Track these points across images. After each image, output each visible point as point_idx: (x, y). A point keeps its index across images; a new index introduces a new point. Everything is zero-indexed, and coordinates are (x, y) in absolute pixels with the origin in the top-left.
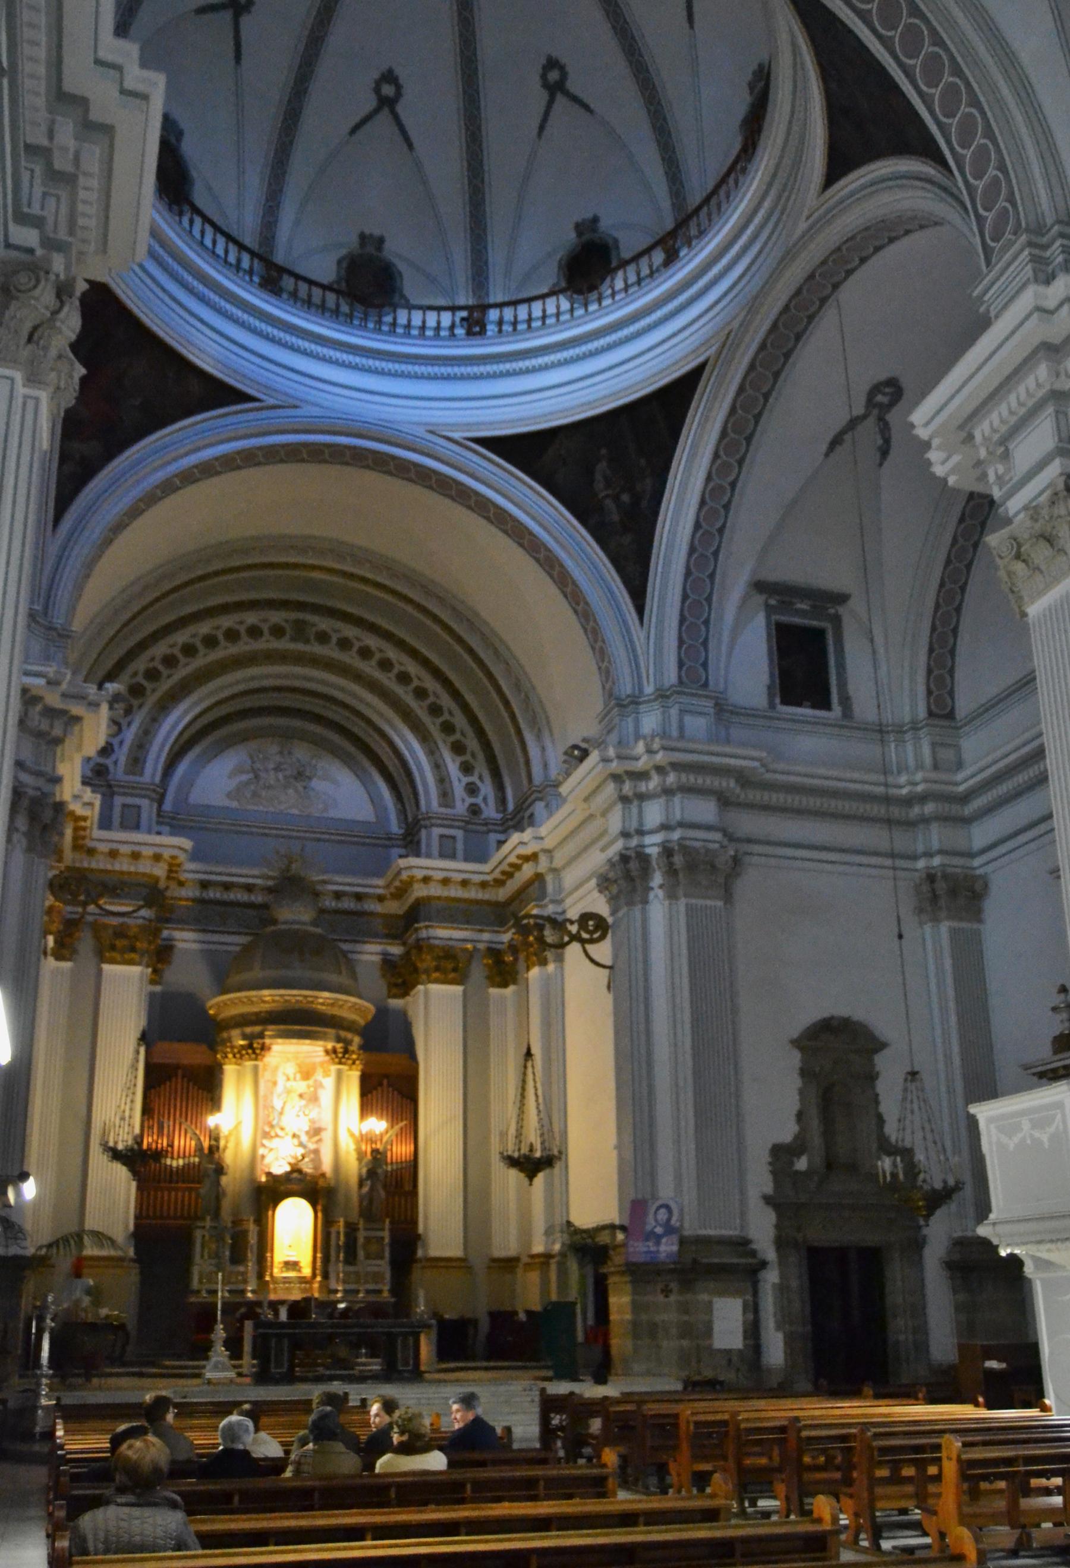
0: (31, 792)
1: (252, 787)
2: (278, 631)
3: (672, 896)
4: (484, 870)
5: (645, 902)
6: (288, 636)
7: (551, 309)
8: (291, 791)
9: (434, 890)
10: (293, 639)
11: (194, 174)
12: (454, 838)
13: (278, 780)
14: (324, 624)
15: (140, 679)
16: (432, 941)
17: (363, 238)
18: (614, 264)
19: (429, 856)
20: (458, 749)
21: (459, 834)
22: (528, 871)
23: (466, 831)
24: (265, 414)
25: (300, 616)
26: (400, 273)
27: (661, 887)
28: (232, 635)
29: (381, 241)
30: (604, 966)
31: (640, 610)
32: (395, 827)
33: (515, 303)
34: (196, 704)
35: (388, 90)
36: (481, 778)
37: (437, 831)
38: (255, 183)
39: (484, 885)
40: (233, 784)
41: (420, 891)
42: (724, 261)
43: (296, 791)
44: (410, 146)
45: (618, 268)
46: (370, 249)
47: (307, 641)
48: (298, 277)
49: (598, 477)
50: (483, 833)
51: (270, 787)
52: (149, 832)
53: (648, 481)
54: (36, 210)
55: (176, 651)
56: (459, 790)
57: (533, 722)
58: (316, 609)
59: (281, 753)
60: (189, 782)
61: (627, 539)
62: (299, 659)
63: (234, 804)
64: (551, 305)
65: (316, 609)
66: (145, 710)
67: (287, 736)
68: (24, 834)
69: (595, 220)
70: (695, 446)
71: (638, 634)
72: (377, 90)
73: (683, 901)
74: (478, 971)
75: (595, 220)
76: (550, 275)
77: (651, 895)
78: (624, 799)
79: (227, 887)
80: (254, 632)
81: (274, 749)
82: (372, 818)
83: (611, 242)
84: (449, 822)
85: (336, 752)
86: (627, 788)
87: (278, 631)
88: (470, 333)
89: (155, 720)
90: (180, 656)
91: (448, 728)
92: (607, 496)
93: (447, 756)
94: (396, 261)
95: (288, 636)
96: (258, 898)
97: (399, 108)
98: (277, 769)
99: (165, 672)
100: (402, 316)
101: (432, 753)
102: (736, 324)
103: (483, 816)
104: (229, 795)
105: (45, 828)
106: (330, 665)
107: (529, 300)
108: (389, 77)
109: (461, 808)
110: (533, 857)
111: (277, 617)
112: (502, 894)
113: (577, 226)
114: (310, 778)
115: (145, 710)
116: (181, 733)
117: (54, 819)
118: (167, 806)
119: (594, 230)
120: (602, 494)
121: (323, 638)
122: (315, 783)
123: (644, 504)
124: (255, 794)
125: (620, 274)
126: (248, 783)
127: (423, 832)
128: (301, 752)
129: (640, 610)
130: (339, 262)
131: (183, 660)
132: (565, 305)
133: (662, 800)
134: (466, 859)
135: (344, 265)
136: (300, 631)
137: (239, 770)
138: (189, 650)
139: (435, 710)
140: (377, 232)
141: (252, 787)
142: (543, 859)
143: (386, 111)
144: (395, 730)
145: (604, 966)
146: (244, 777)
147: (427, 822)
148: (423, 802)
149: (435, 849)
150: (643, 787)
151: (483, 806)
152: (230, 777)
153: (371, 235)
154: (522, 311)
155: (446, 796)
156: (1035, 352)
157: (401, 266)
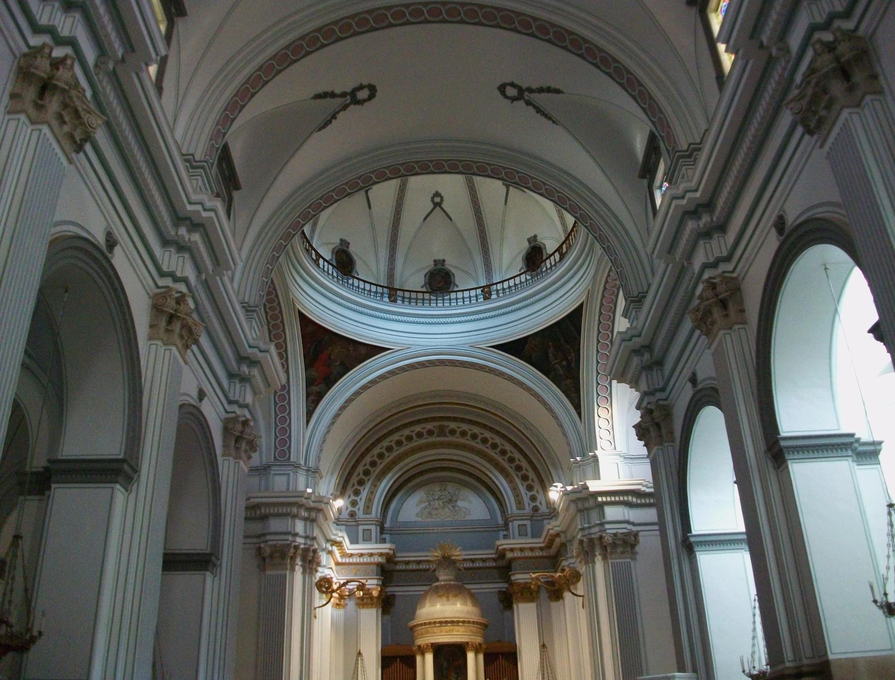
0: (302, 546)
1: (428, 510)
2: (430, 433)
3: (605, 558)
4: (539, 542)
5: (594, 562)
6: (435, 435)
7: (523, 280)
8: (447, 509)
9: (517, 554)
10: (438, 436)
11: (355, 257)
12: (525, 525)
13: (439, 505)
14: (453, 425)
15: (368, 467)
16: (518, 581)
17: (436, 262)
18: (544, 258)
19: (514, 538)
20: (525, 478)
21: (528, 523)
22: (558, 541)
23: (531, 520)
24: (396, 354)
25: (441, 423)
26: (454, 275)
27: (600, 554)
28: (409, 438)
29: (444, 261)
30: (580, 596)
31: (579, 415)
32: (500, 521)
33: (503, 282)
34: (397, 472)
35: (437, 200)
36: (538, 492)
37: (516, 523)
38: (384, 253)
39: (541, 549)
40: (419, 509)
41: (509, 555)
42: (576, 268)
43: (449, 509)
44: (451, 219)
45: (547, 259)
46: (439, 266)
47: (445, 435)
48: (404, 291)
49: (550, 355)
50: (541, 520)
51: (436, 509)
52: (376, 543)
53: (573, 354)
54: (237, 398)
55: (383, 450)
56: (526, 500)
57: (554, 465)
58: (449, 419)
59: (440, 490)
60: (397, 512)
61: (568, 382)
62: (442, 445)
63: (419, 519)
64: (523, 277)
65: (449, 419)
66: (371, 481)
67: (443, 481)
68: (301, 566)
69: (535, 236)
70: (589, 336)
71: (581, 427)
72: (432, 200)
73: (610, 561)
74: (544, 595)
75: (535, 236)
76: (519, 264)
77: (596, 559)
78: (580, 511)
79: (419, 562)
80: (420, 435)
81: (437, 488)
82: (489, 517)
83: (542, 246)
84: (522, 517)
85: (466, 485)
86: (580, 506)
87: (430, 433)
88: (485, 299)
89: (375, 486)
90: (377, 460)
91: (519, 468)
92: (555, 364)
93: (518, 481)
94: (450, 268)
95: (435, 435)
96: (433, 566)
97: (443, 206)
98: (439, 499)
99: (387, 454)
100: (453, 295)
101: (511, 481)
102: (590, 287)
103: (540, 512)
104: (417, 515)
105: (311, 562)
106: (457, 446)
107: (508, 280)
108: (437, 194)
109: (528, 510)
110: (558, 535)
111: (429, 426)
112: (553, 551)
113: (528, 240)
114: (456, 501)
115: (371, 481)
116: (386, 496)
117: (313, 557)
118: (387, 525)
119: (536, 241)
120: (553, 363)
121: (453, 432)
122: (459, 503)
123: (573, 365)
124: (430, 513)
125: (548, 262)
126: (425, 508)
127: (510, 524)
128: (451, 488)
129: (579, 415)
130: (425, 276)
131: (387, 454)
132: (529, 277)
133: (597, 510)
134: (533, 536)
135: (428, 276)
136: (442, 431)
137: (421, 502)
138: (389, 449)
139: (511, 460)
140: (441, 258)
141: (428, 510)
142: (563, 536)
143: (438, 208)
144: (491, 472)
145: (580, 596)
146: (424, 505)
147: (512, 519)
148: (509, 510)
149: (516, 533)
150: (587, 505)
151: (539, 506)
152: (417, 505)
153: (439, 260)
154: (506, 285)
155: (520, 503)
156: (629, 356)
157: (453, 270)
